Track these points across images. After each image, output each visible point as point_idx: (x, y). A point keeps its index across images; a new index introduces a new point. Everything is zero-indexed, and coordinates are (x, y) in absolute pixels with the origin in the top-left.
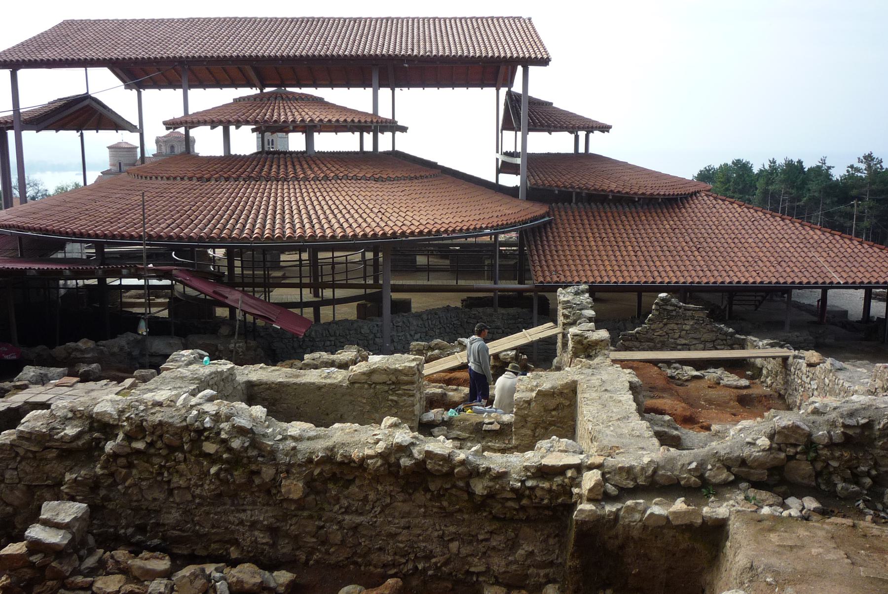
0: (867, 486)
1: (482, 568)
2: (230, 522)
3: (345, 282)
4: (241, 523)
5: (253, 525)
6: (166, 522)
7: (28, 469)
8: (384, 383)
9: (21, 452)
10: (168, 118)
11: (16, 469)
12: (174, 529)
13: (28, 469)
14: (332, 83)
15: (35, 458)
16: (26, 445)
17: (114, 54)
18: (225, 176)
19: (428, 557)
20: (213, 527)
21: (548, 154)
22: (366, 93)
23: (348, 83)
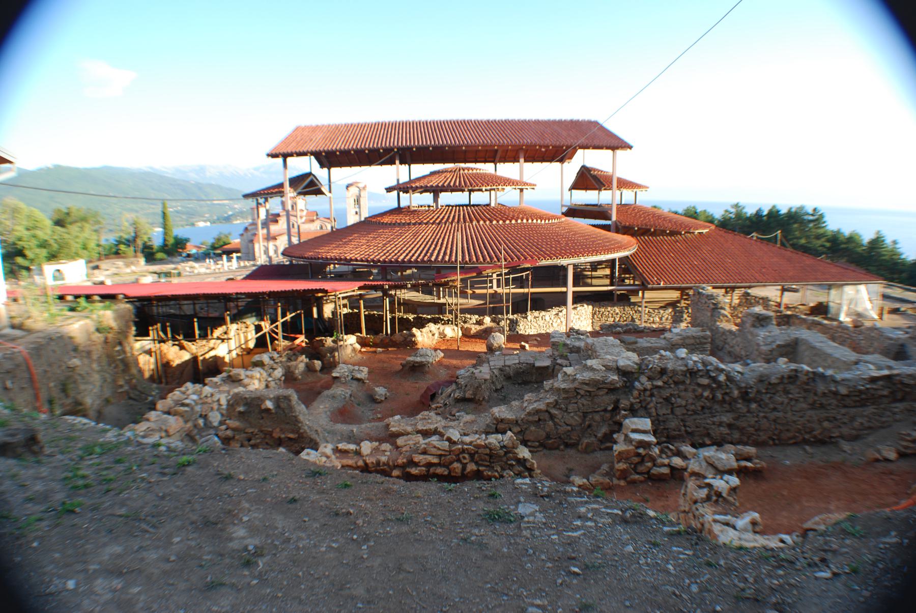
0: (674, 514)
1: (837, 434)
2: (707, 424)
3: (210, 301)
4: (714, 423)
5: (720, 424)
6: (671, 427)
7: (585, 402)
8: (693, 344)
9: (582, 392)
10: (388, 186)
11: (576, 403)
12: (674, 430)
13: (585, 402)
14: (476, 161)
15: (590, 395)
16: (586, 388)
17: (312, 147)
18: (425, 221)
19: (812, 430)
20: (697, 427)
21: (360, 166)
22: (492, 165)
23: (485, 161)
